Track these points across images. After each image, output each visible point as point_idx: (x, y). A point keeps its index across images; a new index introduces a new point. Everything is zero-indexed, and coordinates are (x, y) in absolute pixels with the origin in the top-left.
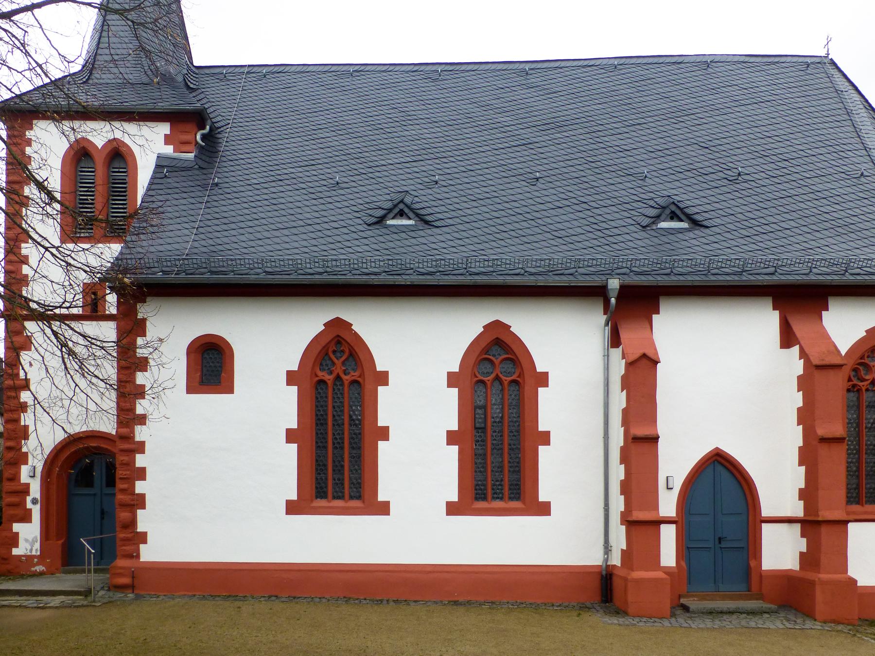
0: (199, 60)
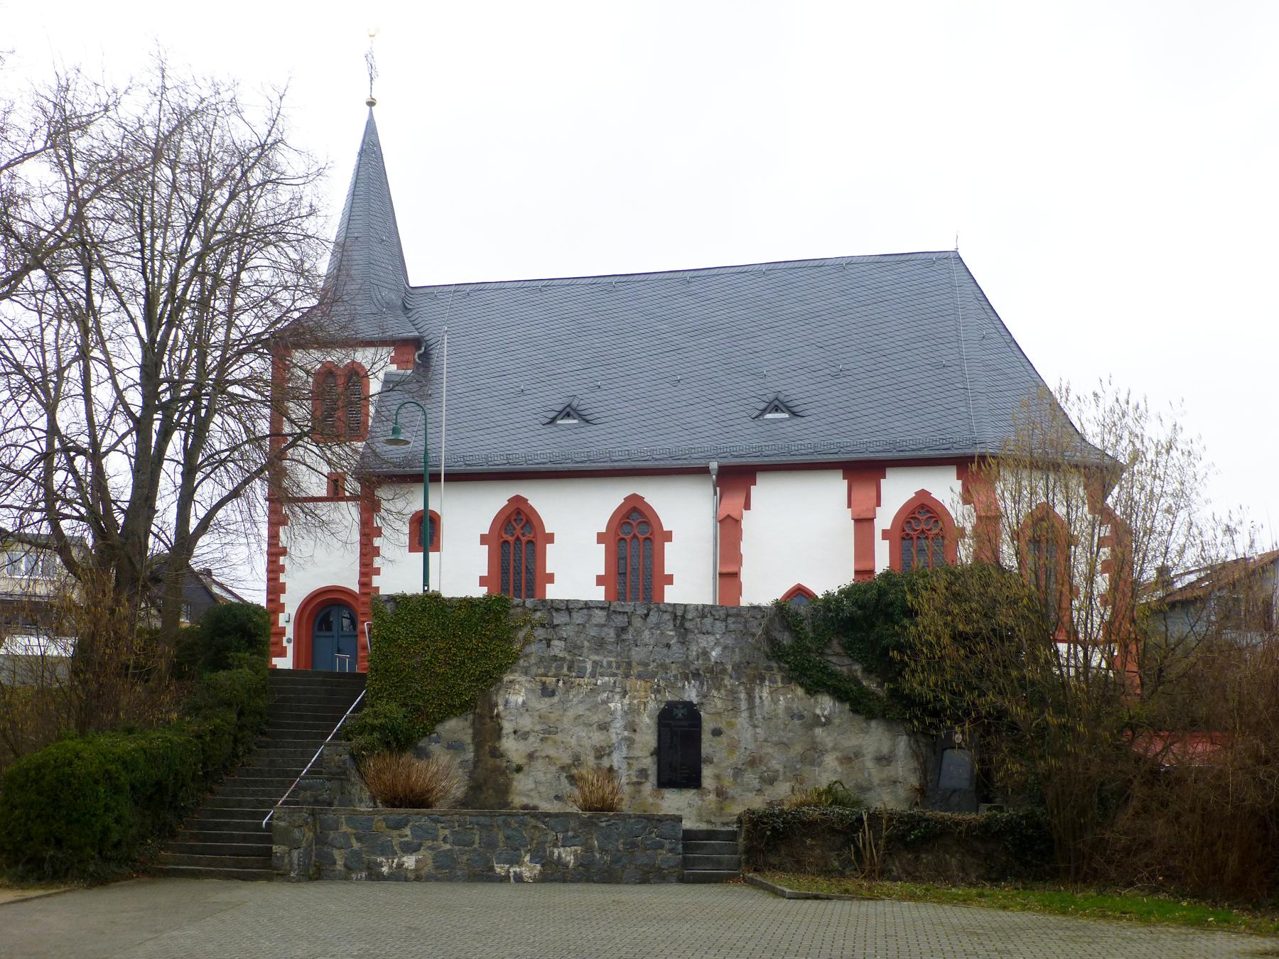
0: (414, 281)
